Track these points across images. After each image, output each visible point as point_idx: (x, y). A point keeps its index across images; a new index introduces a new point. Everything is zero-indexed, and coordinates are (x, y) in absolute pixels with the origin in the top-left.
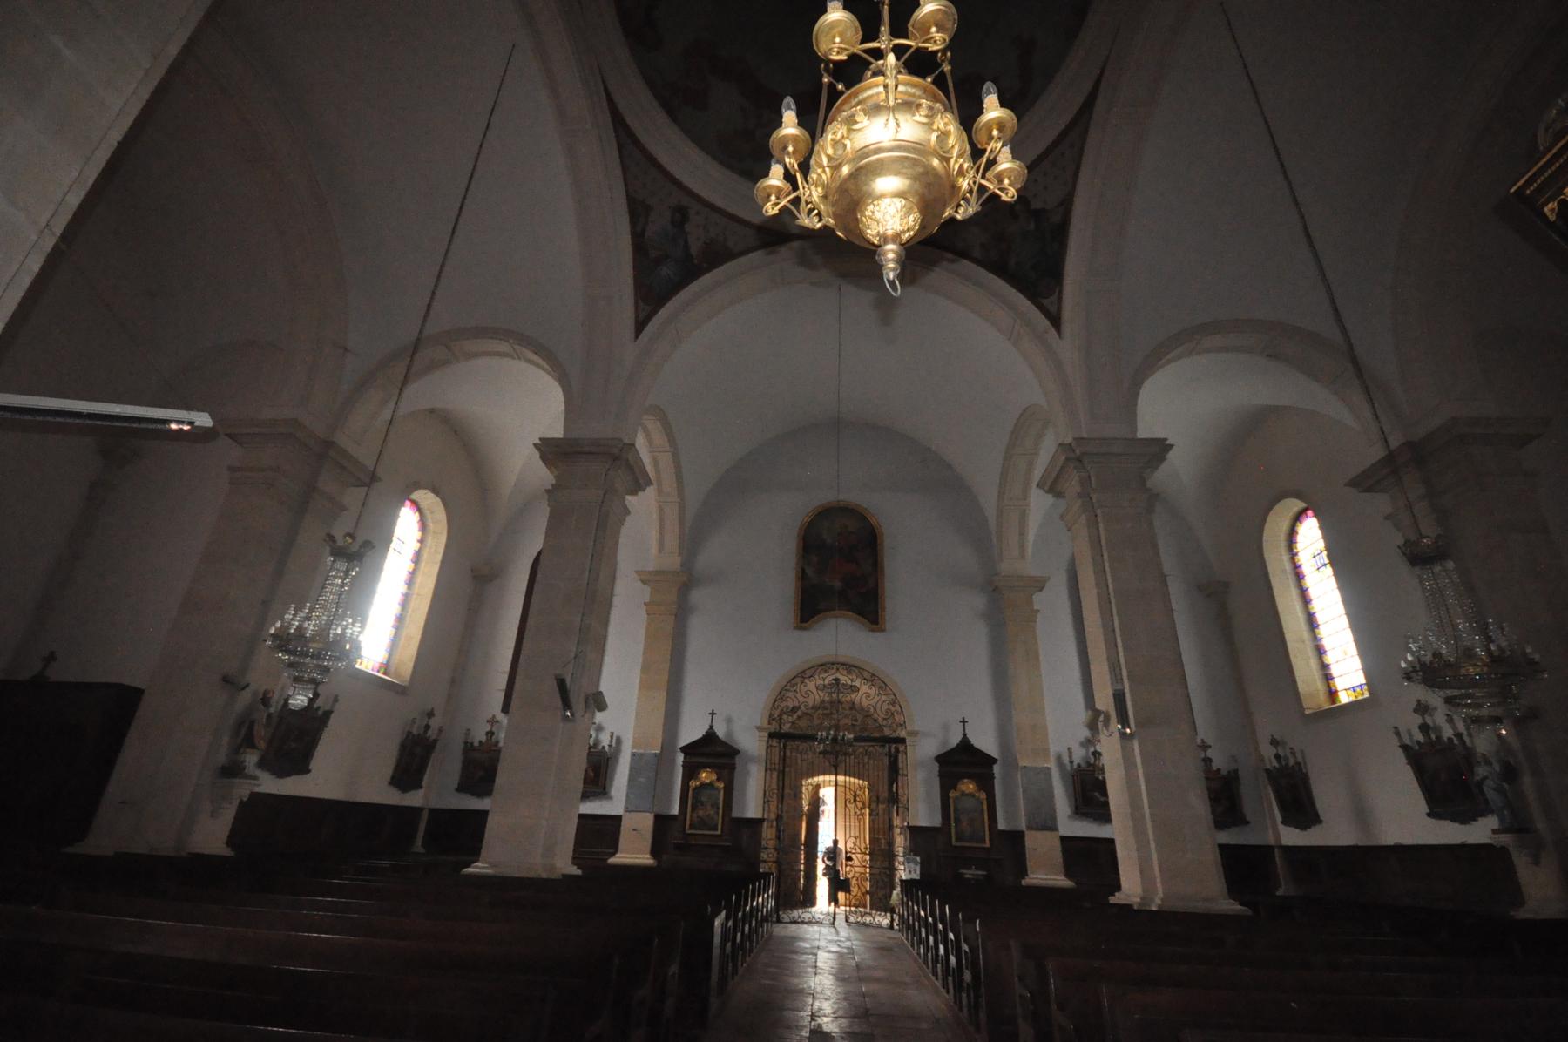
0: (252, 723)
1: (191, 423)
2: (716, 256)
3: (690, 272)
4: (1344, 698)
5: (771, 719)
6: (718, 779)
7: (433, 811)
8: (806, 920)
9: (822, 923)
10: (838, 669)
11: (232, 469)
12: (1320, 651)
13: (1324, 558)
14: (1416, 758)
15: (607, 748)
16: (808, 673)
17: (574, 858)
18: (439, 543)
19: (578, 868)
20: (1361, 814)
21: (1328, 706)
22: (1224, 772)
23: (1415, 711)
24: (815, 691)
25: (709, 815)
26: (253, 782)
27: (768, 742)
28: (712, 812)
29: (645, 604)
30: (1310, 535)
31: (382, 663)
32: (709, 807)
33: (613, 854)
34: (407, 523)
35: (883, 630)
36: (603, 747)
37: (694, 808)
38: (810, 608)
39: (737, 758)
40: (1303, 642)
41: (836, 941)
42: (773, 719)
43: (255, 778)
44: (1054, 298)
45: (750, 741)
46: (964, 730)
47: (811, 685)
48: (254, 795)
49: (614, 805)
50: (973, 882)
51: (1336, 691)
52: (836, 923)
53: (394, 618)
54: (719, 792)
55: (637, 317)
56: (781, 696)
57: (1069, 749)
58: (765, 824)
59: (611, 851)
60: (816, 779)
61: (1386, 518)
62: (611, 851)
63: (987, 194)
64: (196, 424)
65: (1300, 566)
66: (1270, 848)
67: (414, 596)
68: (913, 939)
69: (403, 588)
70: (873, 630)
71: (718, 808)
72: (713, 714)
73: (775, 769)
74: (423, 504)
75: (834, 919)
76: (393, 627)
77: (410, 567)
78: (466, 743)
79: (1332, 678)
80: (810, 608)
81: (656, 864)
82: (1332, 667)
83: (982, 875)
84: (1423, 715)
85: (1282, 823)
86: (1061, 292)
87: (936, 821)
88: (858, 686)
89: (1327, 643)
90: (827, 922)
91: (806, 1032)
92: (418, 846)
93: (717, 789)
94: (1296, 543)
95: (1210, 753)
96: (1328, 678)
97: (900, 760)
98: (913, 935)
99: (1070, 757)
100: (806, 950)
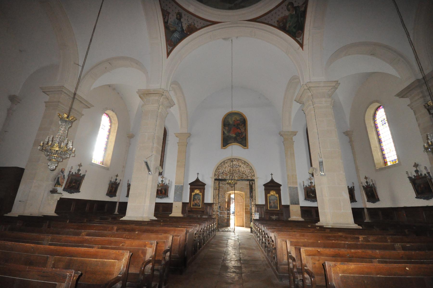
0: (58, 178)
2: (192, 30)
3: (184, 35)
4: (389, 164)
5: (215, 175)
6: (200, 192)
7: (120, 203)
8: (226, 231)
10: (234, 160)
11: (45, 102)
12: (382, 150)
14: (413, 181)
15: (168, 184)
16: (226, 162)
18: (116, 126)
19: (156, 218)
20: (393, 198)
21: (384, 166)
23: (365, 178)
24: (228, 167)
25: (198, 202)
26: (61, 195)
29: (178, 143)
30: (381, 114)
31: (101, 161)
32: (198, 200)
33: (171, 214)
34: (105, 121)
35: (248, 148)
36: (167, 184)
37: (193, 201)
38: (226, 142)
39: (206, 186)
40: (377, 148)
41: (234, 237)
42: (216, 175)
43: (62, 194)
44: (301, 37)
47: (227, 165)
49: (170, 199)
50: (274, 219)
51: (387, 162)
52: (235, 231)
53: (104, 148)
54: (201, 196)
56: (218, 168)
58: (214, 204)
59: (170, 213)
61: (408, 105)
62: (170, 213)
65: (377, 124)
66: (363, 208)
67: (110, 142)
68: (256, 236)
69: (106, 140)
70: (245, 148)
71: (200, 200)
72: (198, 174)
73: (217, 189)
74: (110, 115)
75: (234, 230)
77: (108, 133)
78: (128, 184)
79: (386, 158)
80: (226, 142)
84: (416, 167)
85: (367, 201)
87: (264, 203)
88: (241, 165)
90: (232, 231)
91: (220, 266)
92: (116, 212)
94: (376, 117)
96: (384, 158)
97: (253, 186)
98: (256, 235)
99: (304, 184)
100: (225, 239)
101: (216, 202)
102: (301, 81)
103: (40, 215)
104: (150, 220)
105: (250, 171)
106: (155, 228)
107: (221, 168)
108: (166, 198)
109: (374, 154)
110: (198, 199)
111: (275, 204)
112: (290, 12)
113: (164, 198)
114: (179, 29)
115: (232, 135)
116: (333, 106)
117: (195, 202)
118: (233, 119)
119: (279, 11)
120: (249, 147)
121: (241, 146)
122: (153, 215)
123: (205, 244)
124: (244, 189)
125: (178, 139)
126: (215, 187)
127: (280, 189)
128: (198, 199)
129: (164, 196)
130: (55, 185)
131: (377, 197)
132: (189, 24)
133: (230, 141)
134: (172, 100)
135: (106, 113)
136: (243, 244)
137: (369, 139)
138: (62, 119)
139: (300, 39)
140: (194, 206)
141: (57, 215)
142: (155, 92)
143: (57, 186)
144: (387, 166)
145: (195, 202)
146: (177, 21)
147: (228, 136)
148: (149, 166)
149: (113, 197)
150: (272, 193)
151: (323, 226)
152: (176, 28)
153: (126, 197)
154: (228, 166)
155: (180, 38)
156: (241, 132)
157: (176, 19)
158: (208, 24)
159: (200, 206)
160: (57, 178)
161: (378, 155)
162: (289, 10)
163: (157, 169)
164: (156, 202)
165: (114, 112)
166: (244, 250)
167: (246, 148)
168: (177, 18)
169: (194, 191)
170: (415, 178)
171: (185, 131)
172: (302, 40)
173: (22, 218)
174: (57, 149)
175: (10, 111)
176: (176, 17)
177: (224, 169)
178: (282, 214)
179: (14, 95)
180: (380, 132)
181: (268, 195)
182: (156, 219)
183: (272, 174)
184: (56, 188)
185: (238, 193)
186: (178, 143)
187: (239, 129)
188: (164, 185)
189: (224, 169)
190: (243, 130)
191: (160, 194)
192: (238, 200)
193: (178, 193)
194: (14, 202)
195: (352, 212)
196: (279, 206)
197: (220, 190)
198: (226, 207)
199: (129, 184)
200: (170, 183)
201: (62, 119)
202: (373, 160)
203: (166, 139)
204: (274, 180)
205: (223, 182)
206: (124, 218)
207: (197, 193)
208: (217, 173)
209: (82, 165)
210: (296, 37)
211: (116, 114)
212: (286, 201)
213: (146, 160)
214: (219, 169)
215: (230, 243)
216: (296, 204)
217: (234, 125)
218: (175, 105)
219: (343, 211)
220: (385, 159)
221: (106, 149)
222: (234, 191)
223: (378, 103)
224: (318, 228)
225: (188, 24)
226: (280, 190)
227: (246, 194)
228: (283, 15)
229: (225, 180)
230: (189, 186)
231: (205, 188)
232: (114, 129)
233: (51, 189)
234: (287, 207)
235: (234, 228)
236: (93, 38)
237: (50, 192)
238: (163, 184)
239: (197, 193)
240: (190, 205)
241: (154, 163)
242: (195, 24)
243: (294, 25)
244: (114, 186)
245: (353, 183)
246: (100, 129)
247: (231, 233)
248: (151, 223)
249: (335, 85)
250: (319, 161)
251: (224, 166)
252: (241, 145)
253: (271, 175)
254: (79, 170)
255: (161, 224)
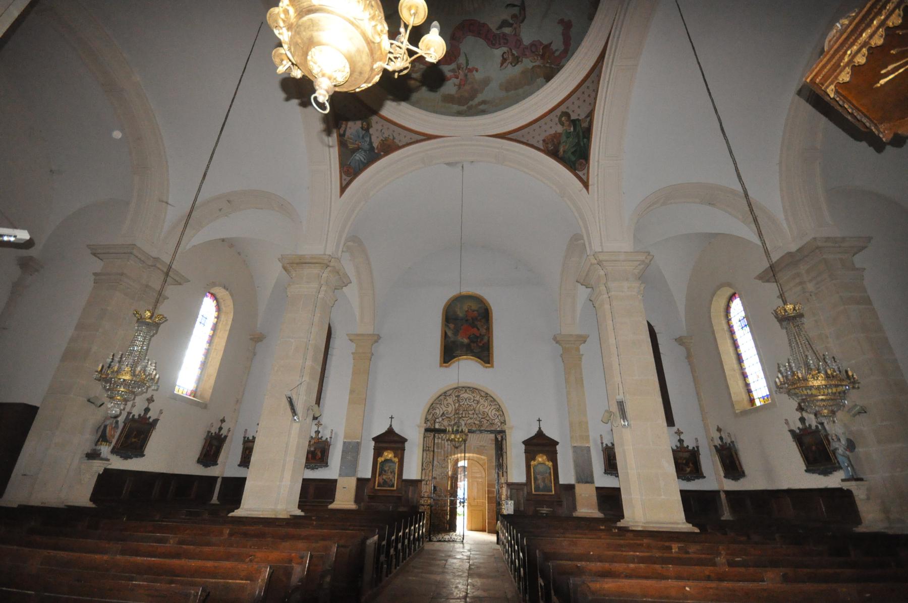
0: (105, 427)
1: (15, 236)
2: (389, 147)
3: (373, 156)
5: (427, 420)
6: (395, 457)
7: (225, 480)
8: (447, 540)
9: (456, 541)
10: (466, 391)
11: (95, 274)
12: (744, 376)
13: (745, 322)
15: (329, 440)
16: (448, 393)
17: (299, 505)
18: (228, 319)
19: (302, 511)
21: (749, 407)
22: (690, 448)
24: (452, 404)
27: (424, 434)
28: (391, 477)
29: (352, 353)
30: (737, 309)
32: (389, 474)
33: (331, 503)
34: (208, 307)
35: (492, 366)
36: (327, 439)
37: (379, 475)
38: (449, 354)
39: (406, 444)
42: (428, 421)
43: (108, 460)
44: (585, 171)
45: (414, 435)
46: (540, 426)
47: (450, 400)
48: (106, 470)
49: (331, 472)
50: (545, 515)
51: (754, 399)
52: (464, 541)
53: (200, 363)
54: (396, 464)
55: (341, 184)
56: (432, 407)
57: (601, 435)
58: (423, 483)
60: (456, 456)
63: (415, 56)
64: (18, 237)
67: (213, 351)
69: (206, 346)
70: (486, 367)
71: (395, 474)
72: (392, 418)
73: (428, 450)
74: (219, 296)
75: (463, 539)
76: (199, 368)
78: (245, 437)
80: (449, 354)
81: (357, 507)
82: (751, 385)
83: (550, 511)
86: (589, 167)
87: (522, 479)
89: (748, 371)
92: (215, 499)
93: (394, 462)
94: (730, 313)
95: (682, 437)
96: (749, 391)
99: (602, 440)
101: (427, 478)
102: (588, 249)
103: (61, 506)
104: (290, 515)
105: (496, 413)
106: (304, 532)
107: (438, 406)
108: (324, 468)
109: (731, 382)
110: (389, 471)
111: (546, 482)
112: (565, 128)
113: (319, 469)
114: (366, 146)
115: (462, 341)
116: (643, 296)
117: (384, 477)
118: (465, 308)
119: (546, 124)
120: (495, 363)
121: (479, 363)
122: (297, 506)
123: (398, 566)
124: (486, 450)
125: (354, 345)
126: (425, 446)
127: (556, 451)
128: (389, 471)
129: (319, 465)
130: (98, 441)
131: (741, 467)
132: (383, 138)
133: (459, 352)
134: (346, 275)
135: (212, 291)
136: (478, 567)
137: (719, 353)
138: (140, 321)
139: (584, 174)
140: (382, 487)
141: (94, 506)
142: (315, 261)
143: (101, 444)
144: (755, 407)
145: (384, 477)
146: (362, 133)
147: (454, 342)
148: (295, 404)
149: (210, 466)
150: (540, 460)
151: (629, 527)
152: (360, 144)
153: (238, 467)
154: (453, 402)
155: (365, 161)
156: (480, 334)
157: (360, 130)
158: (418, 139)
159: (393, 486)
160: (102, 427)
161: (738, 385)
162: (562, 124)
163: (310, 411)
164: (305, 477)
165: (227, 289)
166: (478, 580)
167: (489, 367)
168: (362, 128)
169: (383, 453)
170: (800, 432)
171: (368, 329)
172: (586, 175)
173: (27, 511)
174: (127, 377)
175: (17, 289)
176: (361, 126)
177: (444, 409)
178: (560, 503)
179: (31, 257)
180: (738, 340)
181: (533, 463)
182: (302, 514)
183: (539, 420)
184: (98, 448)
185: (473, 457)
186: (352, 353)
187: (475, 329)
188: (320, 440)
189: (444, 409)
190: (485, 331)
191: (312, 459)
192: (474, 472)
193: (349, 458)
194: (10, 476)
195: (680, 499)
196: (553, 485)
197: (436, 450)
198: (449, 489)
199: (246, 439)
200: (333, 437)
201: (141, 320)
202: (730, 394)
203: (329, 353)
204: (544, 433)
205: (442, 435)
206: (237, 513)
207: (387, 458)
208: (430, 417)
209: (154, 399)
210: (575, 170)
211: (232, 295)
212: (567, 476)
213: (289, 394)
214: (434, 409)
215: (450, 565)
216: (587, 482)
217: (467, 320)
218: (351, 283)
219: (663, 497)
220: (751, 394)
221: (204, 365)
222: (465, 453)
223: (730, 287)
224: (616, 531)
225: (382, 138)
226: (555, 453)
227: (489, 461)
228: (552, 132)
229: (444, 431)
230: (373, 443)
231: (406, 448)
232: (224, 323)
233: (88, 450)
234: (570, 488)
235: (462, 534)
236: (209, 171)
237: (86, 457)
238: (319, 439)
239: (389, 458)
240: (372, 485)
241: (305, 398)
242: (394, 138)
243: (574, 149)
244: (215, 443)
245: (697, 440)
246: (197, 324)
247: (455, 544)
248: (293, 521)
249: (644, 258)
250: (616, 399)
251: (446, 402)
252: (479, 360)
253: (538, 422)
254: (147, 410)
255: (313, 524)
